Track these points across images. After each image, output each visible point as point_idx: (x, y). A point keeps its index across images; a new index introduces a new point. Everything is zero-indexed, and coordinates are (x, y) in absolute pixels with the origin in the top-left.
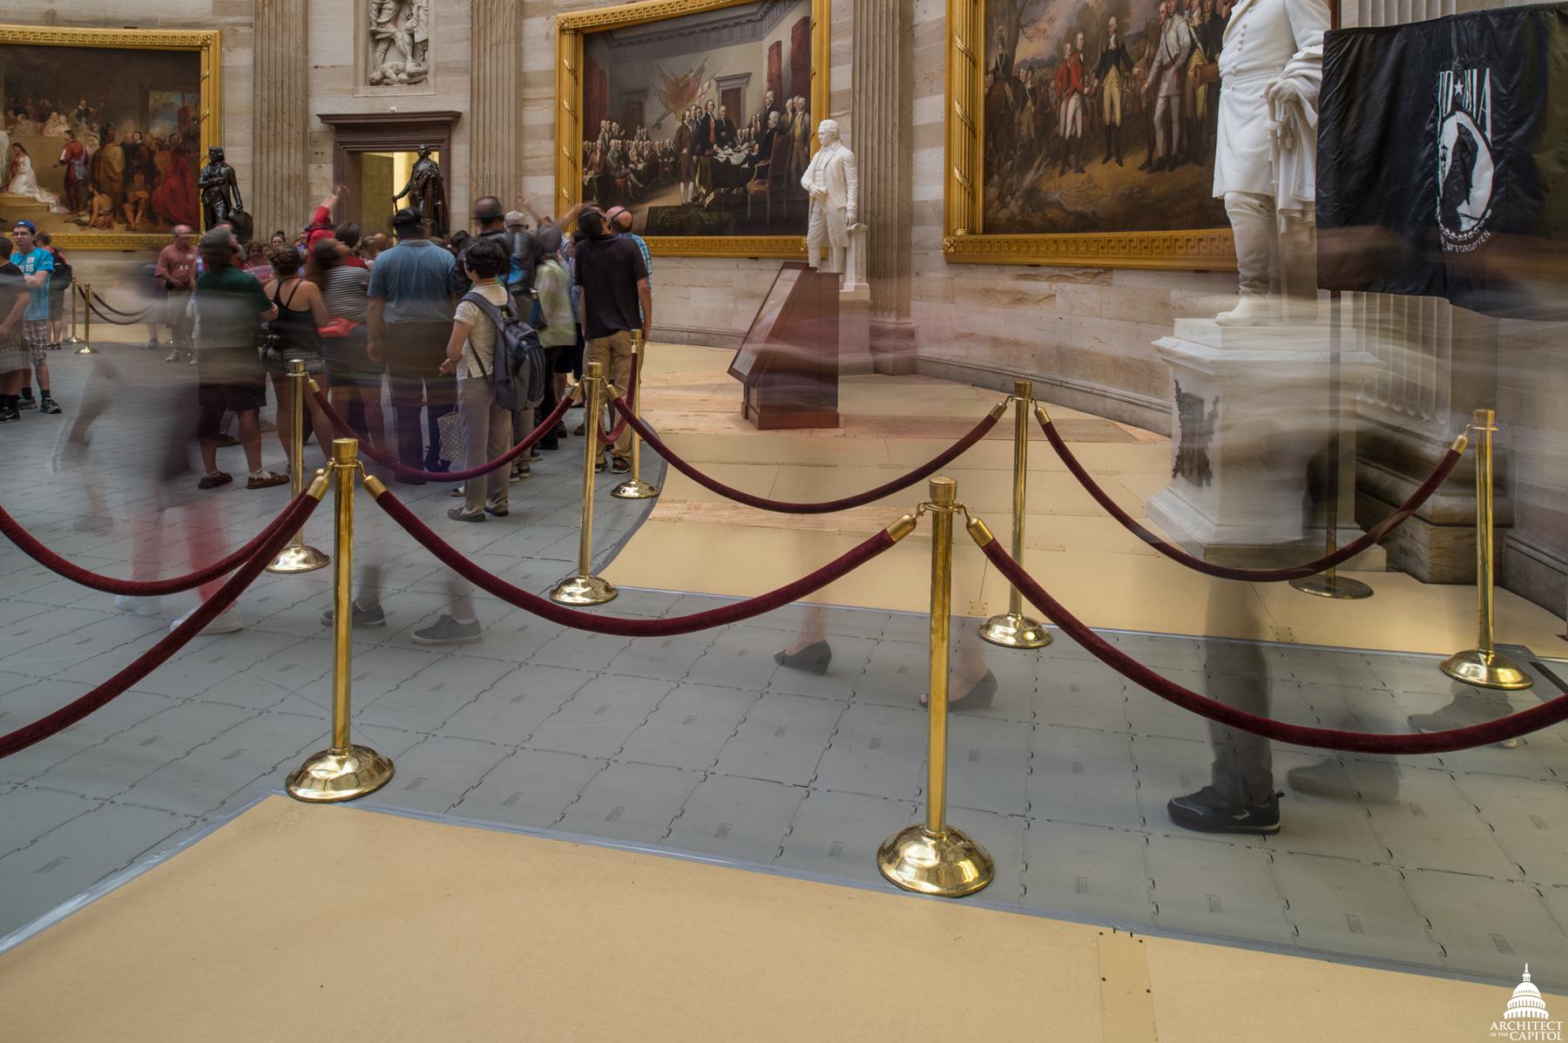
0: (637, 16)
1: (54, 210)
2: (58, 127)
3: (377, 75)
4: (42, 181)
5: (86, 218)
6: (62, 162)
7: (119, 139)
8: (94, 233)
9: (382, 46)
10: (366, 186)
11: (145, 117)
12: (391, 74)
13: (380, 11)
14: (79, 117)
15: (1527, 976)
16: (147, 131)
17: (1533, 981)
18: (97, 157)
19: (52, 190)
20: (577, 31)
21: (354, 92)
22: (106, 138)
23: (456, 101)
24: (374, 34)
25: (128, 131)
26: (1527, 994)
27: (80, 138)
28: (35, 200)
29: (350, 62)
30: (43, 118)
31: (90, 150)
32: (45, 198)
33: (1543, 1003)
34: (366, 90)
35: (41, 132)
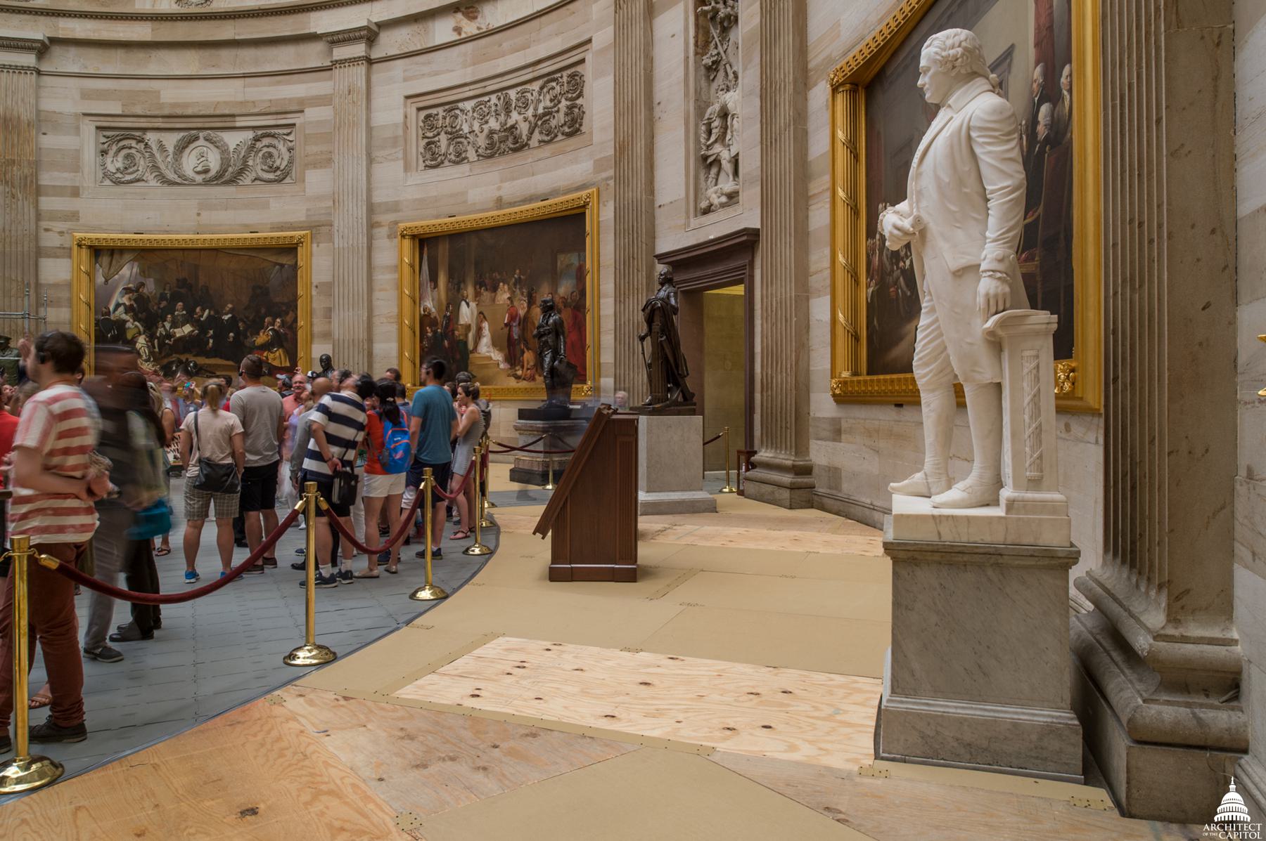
0: (469, 225)
1: (502, 366)
2: (503, 296)
3: (704, 205)
4: (495, 343)
5: (519, 373)
6: (506, 325)
7: (539, 302)
8: (524, 384)
9: (714, 170)
10: (709, 328)
11: (555, 279)
12: (716, 201)
13: (709, 133)
14: (515, 285)
15: (1232, 787)
16: (556, 291)
17: (1237, 791)
18: (527, 317)
19: (501, 350)
20: (413, 237)
21: (687, 224)
22: (531, 302)
23: (747, 216)
24: (705, 158)
25: (544, 294)
26: (1232, 801)
27: (516, 303)
28: (490, 358)
29: (683, 194)
30: (495, 289)
31: (522, 313)
32: (497, 356)
33: (1246, 809)
34: (694, 222)
35: (494, 300)
